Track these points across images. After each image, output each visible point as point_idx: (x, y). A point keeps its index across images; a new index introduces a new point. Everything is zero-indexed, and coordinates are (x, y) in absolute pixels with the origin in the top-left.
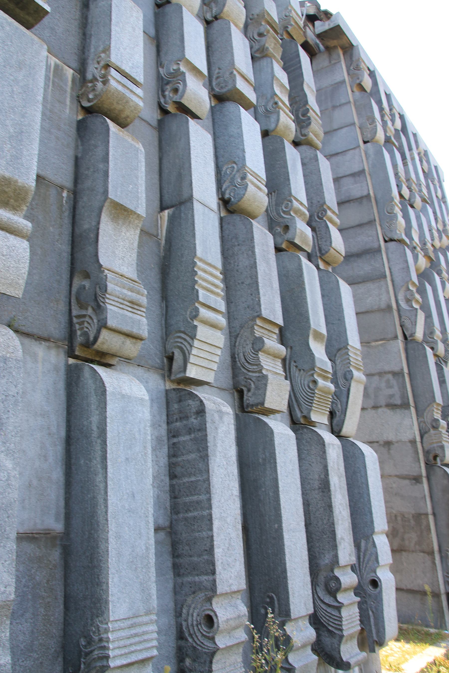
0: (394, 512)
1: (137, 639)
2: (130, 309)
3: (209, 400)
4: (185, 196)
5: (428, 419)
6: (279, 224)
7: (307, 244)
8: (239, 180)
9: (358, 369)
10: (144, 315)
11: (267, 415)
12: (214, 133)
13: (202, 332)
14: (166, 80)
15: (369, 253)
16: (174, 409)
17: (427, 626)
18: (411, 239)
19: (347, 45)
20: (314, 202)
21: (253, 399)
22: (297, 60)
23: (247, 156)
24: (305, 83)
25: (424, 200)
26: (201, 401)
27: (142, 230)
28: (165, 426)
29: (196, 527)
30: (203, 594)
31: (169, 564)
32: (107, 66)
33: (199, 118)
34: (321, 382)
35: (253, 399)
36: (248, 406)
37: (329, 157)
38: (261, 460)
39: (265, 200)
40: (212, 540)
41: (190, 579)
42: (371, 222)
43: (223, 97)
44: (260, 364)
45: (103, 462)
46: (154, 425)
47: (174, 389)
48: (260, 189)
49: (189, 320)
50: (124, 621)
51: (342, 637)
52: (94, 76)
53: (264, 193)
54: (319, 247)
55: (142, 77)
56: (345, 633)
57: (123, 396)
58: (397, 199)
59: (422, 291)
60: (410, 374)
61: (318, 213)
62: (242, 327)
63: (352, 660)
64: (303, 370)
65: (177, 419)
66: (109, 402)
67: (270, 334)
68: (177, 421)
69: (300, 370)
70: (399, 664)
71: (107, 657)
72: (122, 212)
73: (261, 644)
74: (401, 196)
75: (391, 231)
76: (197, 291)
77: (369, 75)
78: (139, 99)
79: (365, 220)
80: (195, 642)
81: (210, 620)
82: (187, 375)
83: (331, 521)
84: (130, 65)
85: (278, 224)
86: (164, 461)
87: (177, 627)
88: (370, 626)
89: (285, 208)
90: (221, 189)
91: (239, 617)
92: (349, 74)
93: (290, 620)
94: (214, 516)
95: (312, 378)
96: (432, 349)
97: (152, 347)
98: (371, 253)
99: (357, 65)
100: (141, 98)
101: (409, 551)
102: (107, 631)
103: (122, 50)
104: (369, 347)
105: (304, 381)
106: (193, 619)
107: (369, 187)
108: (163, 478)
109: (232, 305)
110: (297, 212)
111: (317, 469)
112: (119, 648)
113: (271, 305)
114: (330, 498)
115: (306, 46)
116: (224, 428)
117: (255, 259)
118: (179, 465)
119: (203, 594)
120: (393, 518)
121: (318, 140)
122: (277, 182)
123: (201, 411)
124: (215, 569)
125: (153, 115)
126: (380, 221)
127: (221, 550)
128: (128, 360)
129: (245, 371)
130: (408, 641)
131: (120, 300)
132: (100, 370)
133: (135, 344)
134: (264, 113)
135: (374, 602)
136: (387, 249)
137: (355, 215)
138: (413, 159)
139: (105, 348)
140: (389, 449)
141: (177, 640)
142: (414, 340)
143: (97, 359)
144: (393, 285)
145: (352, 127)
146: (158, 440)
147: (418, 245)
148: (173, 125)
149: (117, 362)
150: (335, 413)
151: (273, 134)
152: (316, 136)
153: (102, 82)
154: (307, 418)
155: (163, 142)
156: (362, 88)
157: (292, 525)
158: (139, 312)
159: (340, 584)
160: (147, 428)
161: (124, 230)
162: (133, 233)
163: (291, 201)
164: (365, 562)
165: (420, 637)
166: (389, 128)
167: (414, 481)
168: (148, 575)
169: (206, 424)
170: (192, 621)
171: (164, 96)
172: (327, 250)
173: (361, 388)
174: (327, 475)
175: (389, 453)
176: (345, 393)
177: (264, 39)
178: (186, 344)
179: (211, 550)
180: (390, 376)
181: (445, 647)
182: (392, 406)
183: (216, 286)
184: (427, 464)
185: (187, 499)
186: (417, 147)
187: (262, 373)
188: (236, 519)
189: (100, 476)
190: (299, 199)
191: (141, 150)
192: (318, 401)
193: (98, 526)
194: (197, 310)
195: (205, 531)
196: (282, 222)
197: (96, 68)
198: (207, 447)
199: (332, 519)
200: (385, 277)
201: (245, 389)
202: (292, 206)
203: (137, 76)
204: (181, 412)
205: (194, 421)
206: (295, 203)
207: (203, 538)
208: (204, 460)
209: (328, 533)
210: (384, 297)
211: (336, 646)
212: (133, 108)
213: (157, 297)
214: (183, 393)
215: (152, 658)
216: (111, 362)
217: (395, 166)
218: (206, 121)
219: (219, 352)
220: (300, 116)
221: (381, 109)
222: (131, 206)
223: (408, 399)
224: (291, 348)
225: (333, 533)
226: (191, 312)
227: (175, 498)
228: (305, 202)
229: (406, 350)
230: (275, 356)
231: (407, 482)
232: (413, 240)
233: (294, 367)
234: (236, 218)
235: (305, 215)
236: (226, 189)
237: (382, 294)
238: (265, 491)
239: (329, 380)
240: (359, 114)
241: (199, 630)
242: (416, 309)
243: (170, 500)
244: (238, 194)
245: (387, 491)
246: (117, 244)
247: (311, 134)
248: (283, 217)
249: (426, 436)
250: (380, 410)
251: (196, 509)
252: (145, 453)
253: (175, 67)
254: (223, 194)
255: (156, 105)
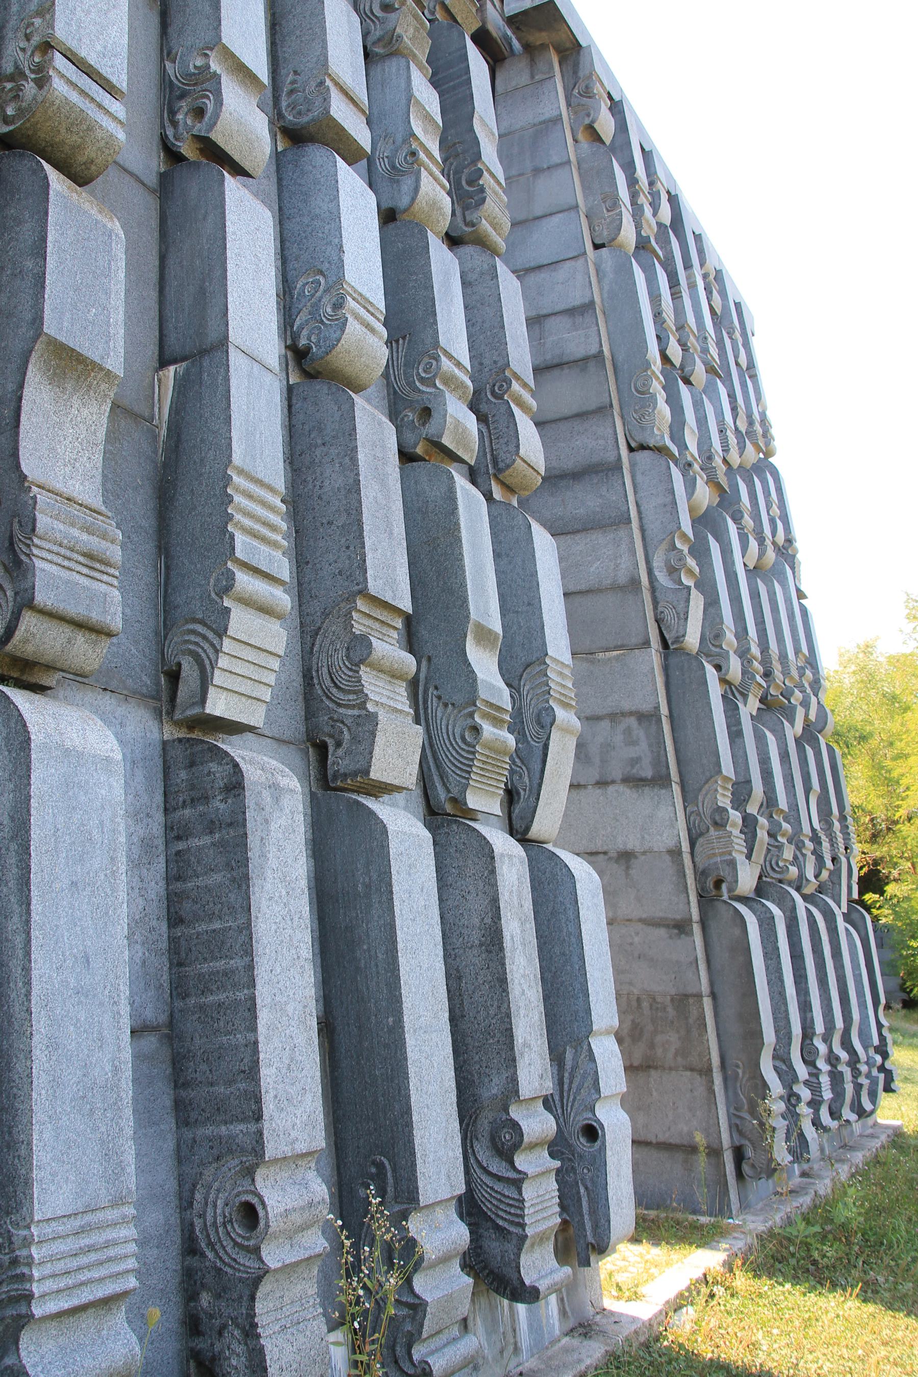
0: (636, 992)
1: (93, 1257)
2: (85, 571)
3: (251, 762)
4: (213, 336)
5: (706, 808)
6: (410, 405)
7: (467, 448)
8: (329, 310)
9: (566, 706)
10: (116, 583)
11: (376, 797)
12: (280, 209)
13: (241, 622)
14: (179, 88)
15: (597, 473)
16: (179, 781)
17: (694, 1212)
18: (683, 447)
19: (568, 45)
20: (486, 362)
21: (346, 762)
22: (462, 66)
23: (348, 259)
24: (476, 115)
25: (711, 370)
26: (236, 765)
27: (115, 406)
28: (159, 817)
29: (222, 1024)
30: (237, 1161)
31: (168, 1102)
32: (47, 47)
33: (248, 175)
34: (488, 730)
35: (346, 762)
36: (335, 776)
37: (521, 273)
38: (360, 888)
39: (383, 353)
40: (256, 1052)
41: (209, 1130)
42: (604, 410)
43: (302, 134)
44: (362, 691)
45: (21, 890)
46: (136, 814)
47: (180, 740)
48: (372, 330)
49: (213, 595)
50: (65, 1220)
51: (523, 1238)
52: (17, 67)
53: (381, 338)
54: (492, 455)
55: (124, 77)
56: (529, 1231)
57: (67, 752)
58: (657, 365)
59: (700, 551)
60: (671, 716)
61: (494, 385)
62: (326, 614)
63: (541, 1282)
64: (453, 704)
65: (184, 802)
66: (34, 764)
67: (385, 630)
68: (184, 805)
69: (446, 705)
70: (637, 1286)
71: (28, 1297)
72: (72, 365)
73: (357, 1257)
74: (665, 359)
75: (643, 429)
76: (232, 537)
77: (610, 109)
78: (118, 125)
79: (592, 405)
80: (220, 1258)
81: (250, 1214)
82: (207, 711)
83: (503, 1010)
84: (99, 48)
85: (410, 406)
86: (156, 888)
87: (182, 1230)
88: (582, 1216)
89: (425, 371)
90: (292, 327)
91: (311, 1204)
92: (569, 105)
93: (418, 1208)
94: (259, 1001)
95: (469, 721)
96: (718, 668)
97: (134, 651)
98: (602, 471)
99: (587, 87)
100: (120, 122)
101: (663, 1068)
102: (27, 1242)
103: (79, 13)
104: (592, 662)
105: (454, 726)
106: (215, 1213)
107: (599, 337)
108: (154, 923)
109: (308, 569)
110: (449, 380)
111: (477, 904)
112: (54, 1276)
113: (388, 570)
114: (503, 965)
115: (482, 39)
116: (282, 822)
117: (358, 474)
118: (188, 897)
119: (237, 1161)
120: (634, 1004)
121: (499, 234)
122: (408, 318)
123: (235, 785)
124: (260, 1109)
125: (147, 162)
126: (621, 408)
127: (274, 1070)
128: (80, 677)
129: (331, 705)
130: (656, 1241)
131: (63, 551)
132: (20, 698)
133: (95, 643)
134: (388, 173)
135: (589, 1170)
136: (633, 465)
137: (569, 394)
138: (692, 286)
139: (29, 651)
140: (628, 868)
141: (183, 1256)
142: (683, 649)
143: (15, 675)
144: (644, 539)
145: (573, 214)
146: (146, 845)
147: (695, 460)
148: (191, 186)
149: (58, 681)
150: (518, 794)
151: (405, 217)
152: (495, 226)
153: (34, 80)
154: (458, 802)
155: (170, 222)
156: (595, 137)
157: (423, 1019)
158: (105, 578)
159: (522, 1135)
160: (118, 820)
161: (76, 402)
162: (95, 410)
163: (437, 359)
164: (574, 1090)
165: (680, 1234)
166: (647, 221)
167: (676, 931)
168: (117, 1124)
169: (244, 813)
170: (215, 1217)
171: (174, 124)
172: (508, 461)
173: (572, 744)
174: (497, 916)
175: (627, 875)
176: (539, 753)
177: (393, 16)
178: (206, 646)
179: (252, 1072)
180: (632, 721)
181: (725, 1250)
182: (635, 782)
183: (273, 528)
184: (701, 896)
185: (205, 968)
186: (702, 265)
187: (366, 709)
188: (305, 1007)
189: (16, 919)
190: (455, 355)
191: (117, 235)
192: (482, 769)
193: (10, 1023)
194: (231, 577)
195: (240, 1032)
196: (417, 401)
197: (23, 50)
198: (247, 859)
199: (506, 1005)
200: (629, 521)
201: (330, 742)
202: (439, 367)
203: (113, 74)
204: (193, 787)
205: (219, 805)
206: (445, 362)
207: (236, 1047)
208: (240, 886)
209: (498, 1035)
210: (625, 563)
211: (512, 1257)
212: (102, 143)
213: (149, 547)
214: (199, 748)
215: (125, 1294)
216: (46, 681)
217: (655, 298)
218: (265, 181)
219: (275, 664)
220: (464, 183)
221: (632, 182)
222: (93, 354)
223: (668, 768)
224: (429, 659)
225: (509, 1034)
226: (218, 580)
227: (180, 964)
228: (467, 363)
229: (666, 669)
230: (394, 675)
231: (662, 932)
232: (687, 448)
233: (434, 699)
234: (321, 388)
235: (466, 387)
236: (301, 328)
237: (617, 556)
238: (369, 950)
239: (506, 726)
240: (586, 188)
241: (228, 1233)
242: (689, 588)
243: (170, 968)
244: (326, 339)
245: (621, 951)
246: (60, 432)
247: (484, 221)
248: (423, 392)
249: (701, 840)
250: (611, 789)
251: (222, 988)
252: (113, 872)
253: (199, 62)
254: (295, 337)
255: (156, 139)
